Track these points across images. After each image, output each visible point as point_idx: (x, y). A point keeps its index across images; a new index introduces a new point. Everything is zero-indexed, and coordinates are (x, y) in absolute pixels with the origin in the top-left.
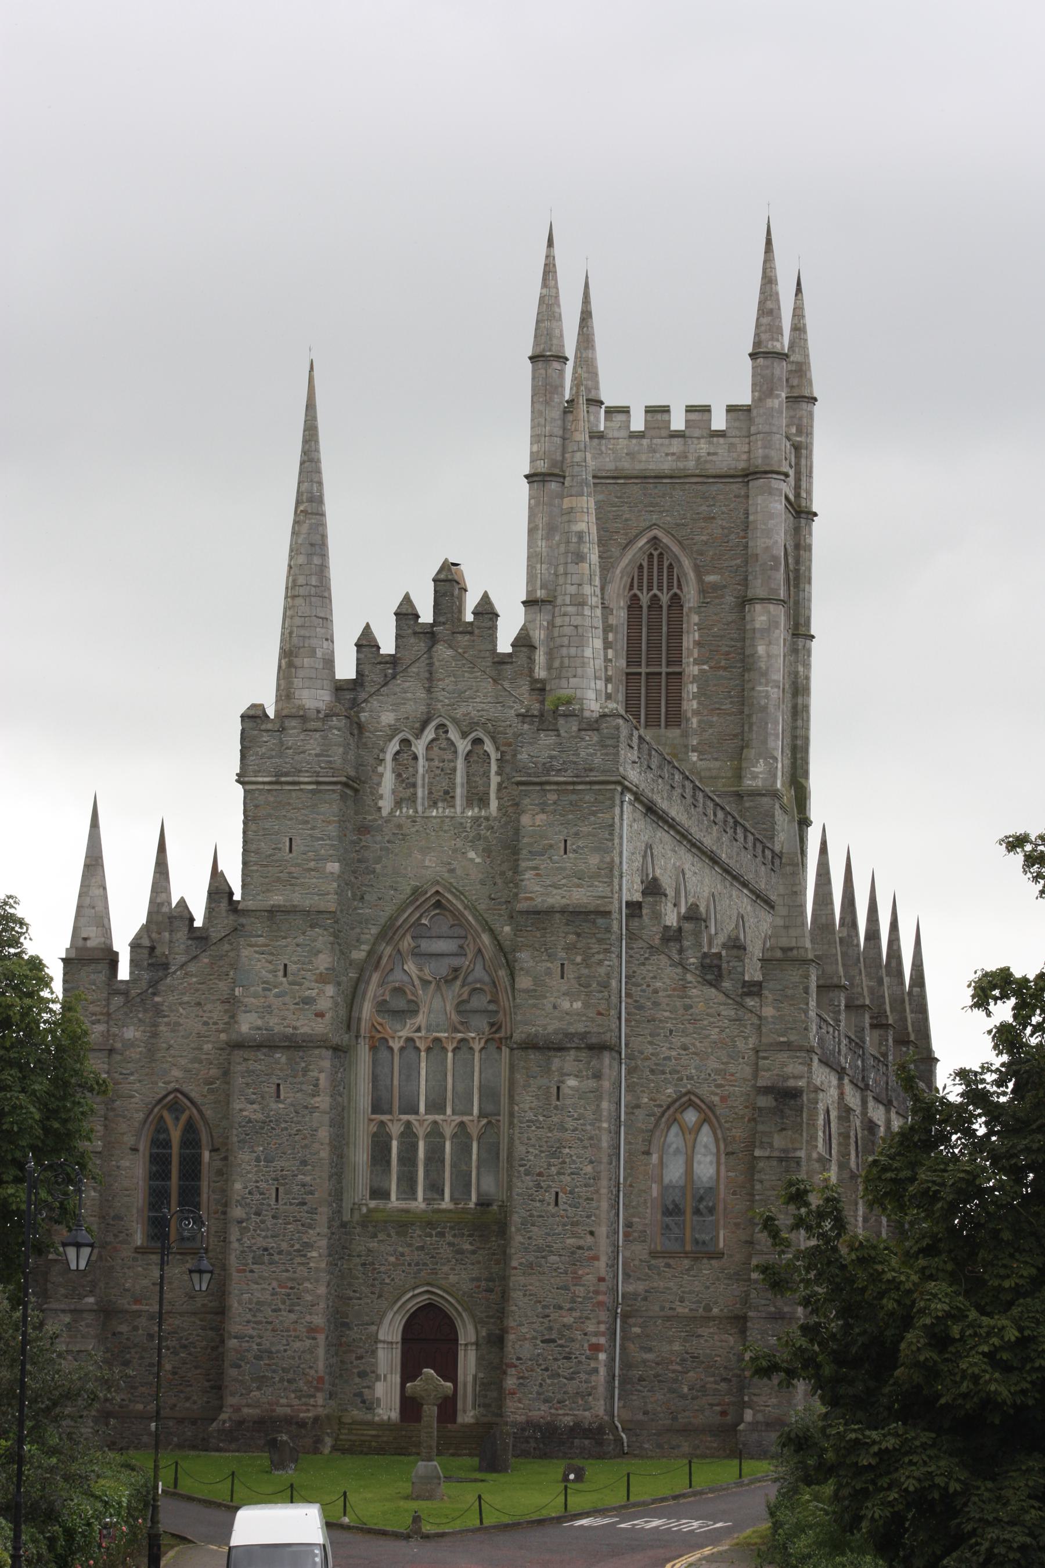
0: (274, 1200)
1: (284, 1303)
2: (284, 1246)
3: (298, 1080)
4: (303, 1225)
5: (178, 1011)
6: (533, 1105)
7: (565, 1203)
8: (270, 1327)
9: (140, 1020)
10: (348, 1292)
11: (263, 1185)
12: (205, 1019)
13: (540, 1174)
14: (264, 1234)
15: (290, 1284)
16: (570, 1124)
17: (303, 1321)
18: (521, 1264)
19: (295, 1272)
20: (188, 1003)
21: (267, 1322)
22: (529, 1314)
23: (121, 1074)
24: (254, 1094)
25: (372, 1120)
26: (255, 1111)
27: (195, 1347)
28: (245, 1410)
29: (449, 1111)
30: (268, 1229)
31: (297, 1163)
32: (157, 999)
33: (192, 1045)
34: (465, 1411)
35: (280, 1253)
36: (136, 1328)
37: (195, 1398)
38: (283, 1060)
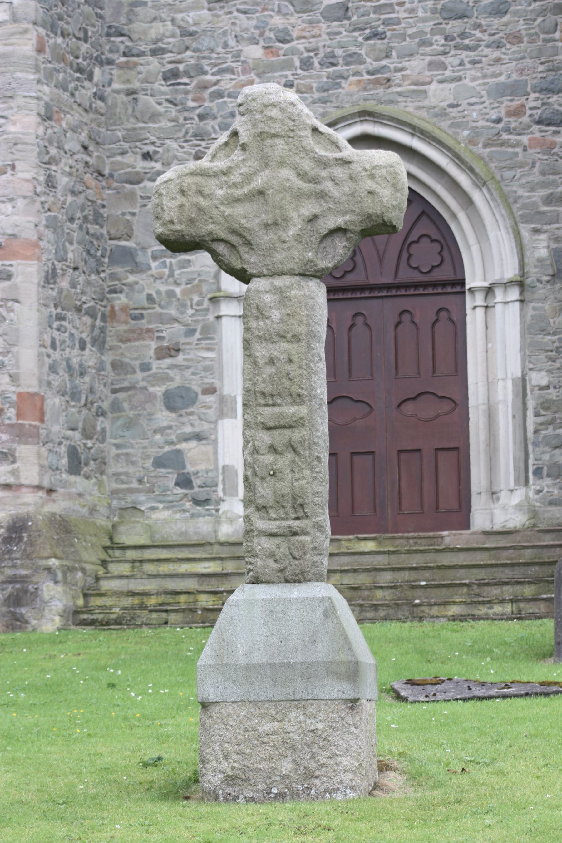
10: (128, 159)
34: (493, 494)
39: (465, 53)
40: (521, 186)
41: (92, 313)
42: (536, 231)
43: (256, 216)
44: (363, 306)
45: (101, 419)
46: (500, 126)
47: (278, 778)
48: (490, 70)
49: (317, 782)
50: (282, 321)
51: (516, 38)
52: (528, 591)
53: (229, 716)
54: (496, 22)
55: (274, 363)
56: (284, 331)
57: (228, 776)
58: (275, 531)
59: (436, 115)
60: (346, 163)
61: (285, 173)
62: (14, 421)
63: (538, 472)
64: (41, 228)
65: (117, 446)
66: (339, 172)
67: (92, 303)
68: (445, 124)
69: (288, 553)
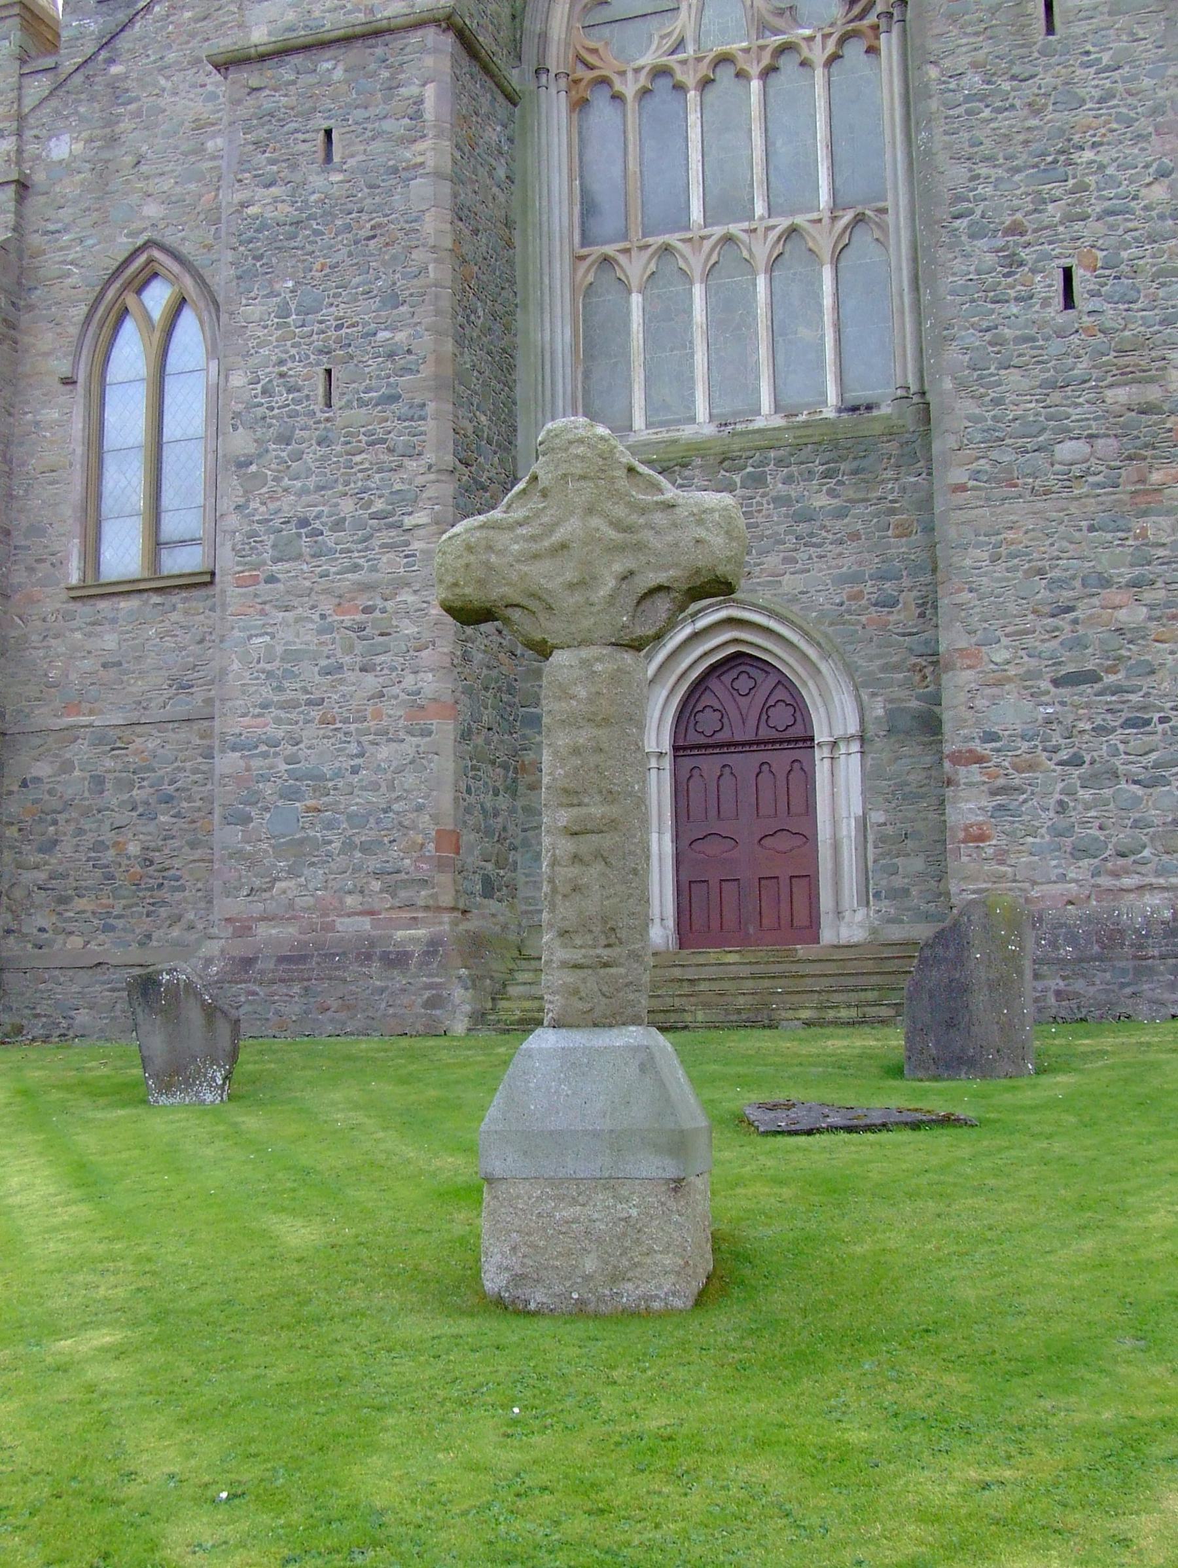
0: (321, 399)
1: (349, 649)
2: (347, 507)
3: (372, 112)
4: (391, 450)
5: (155, 85)
6: (980, 55)
7: (1094, 294)
8: (315, 713)
9: (82, 119)
11: (295, 369)
12: (210, 88)
13: (1016, 229)
14: (298, 484)
15: (363, 601)
16: (1090, 85)
17: (396, 690)
18: (976, 475)
19: (374, 569)
20: (177, 62)
21: (309, 703)
22: (1012, 608)
23: (46, 233)
24: (272, 162)
25: (582, 258)
26: (276, 200)
27: (189, 799)
28: (265, 931)
29: (760, 209)
30: (309, 473)
31: (375, 304)
32: (115, 70)
33: (184, 147)
34: (839, 914)
35: (338, 525)
36: (67, 767)
37: (191, 916)
38: (339, 74)
39: (812, 549)
40: (860, 657)
41: (505, 767)
42: (874, 695)
43: (558, 574)
44: (730, 759)
45: (513, 852)
46: (843, 608)
47: (579, 1280)
48: (834, 563)
49: (630, 1286)
50: (590, 701)
51: (855, 536)
52: (871, 996)
53: (518, 1197)
54: (839, 524)
55: (580, 754)
56: (593, 713)
57: (516, 1275)
58: (581, 961)
59: (789, 601)
60: (670, 506)
61: (595, 521)
62: (433, 853)
63: (877, 895)
64: (458, 694)
65: (527, 875)
66: (659, 518)
67: (505, 758)
68: (796, 608)
69: (596, 989)
